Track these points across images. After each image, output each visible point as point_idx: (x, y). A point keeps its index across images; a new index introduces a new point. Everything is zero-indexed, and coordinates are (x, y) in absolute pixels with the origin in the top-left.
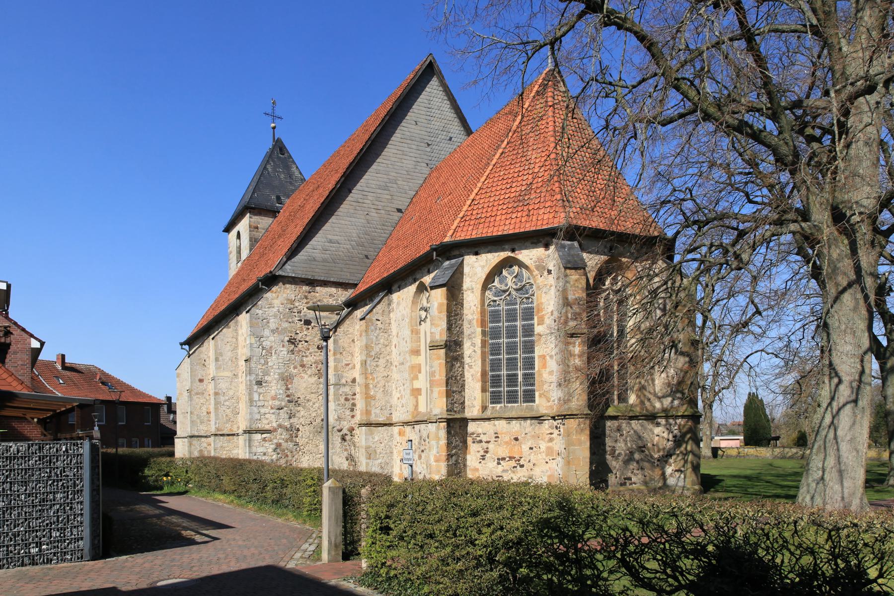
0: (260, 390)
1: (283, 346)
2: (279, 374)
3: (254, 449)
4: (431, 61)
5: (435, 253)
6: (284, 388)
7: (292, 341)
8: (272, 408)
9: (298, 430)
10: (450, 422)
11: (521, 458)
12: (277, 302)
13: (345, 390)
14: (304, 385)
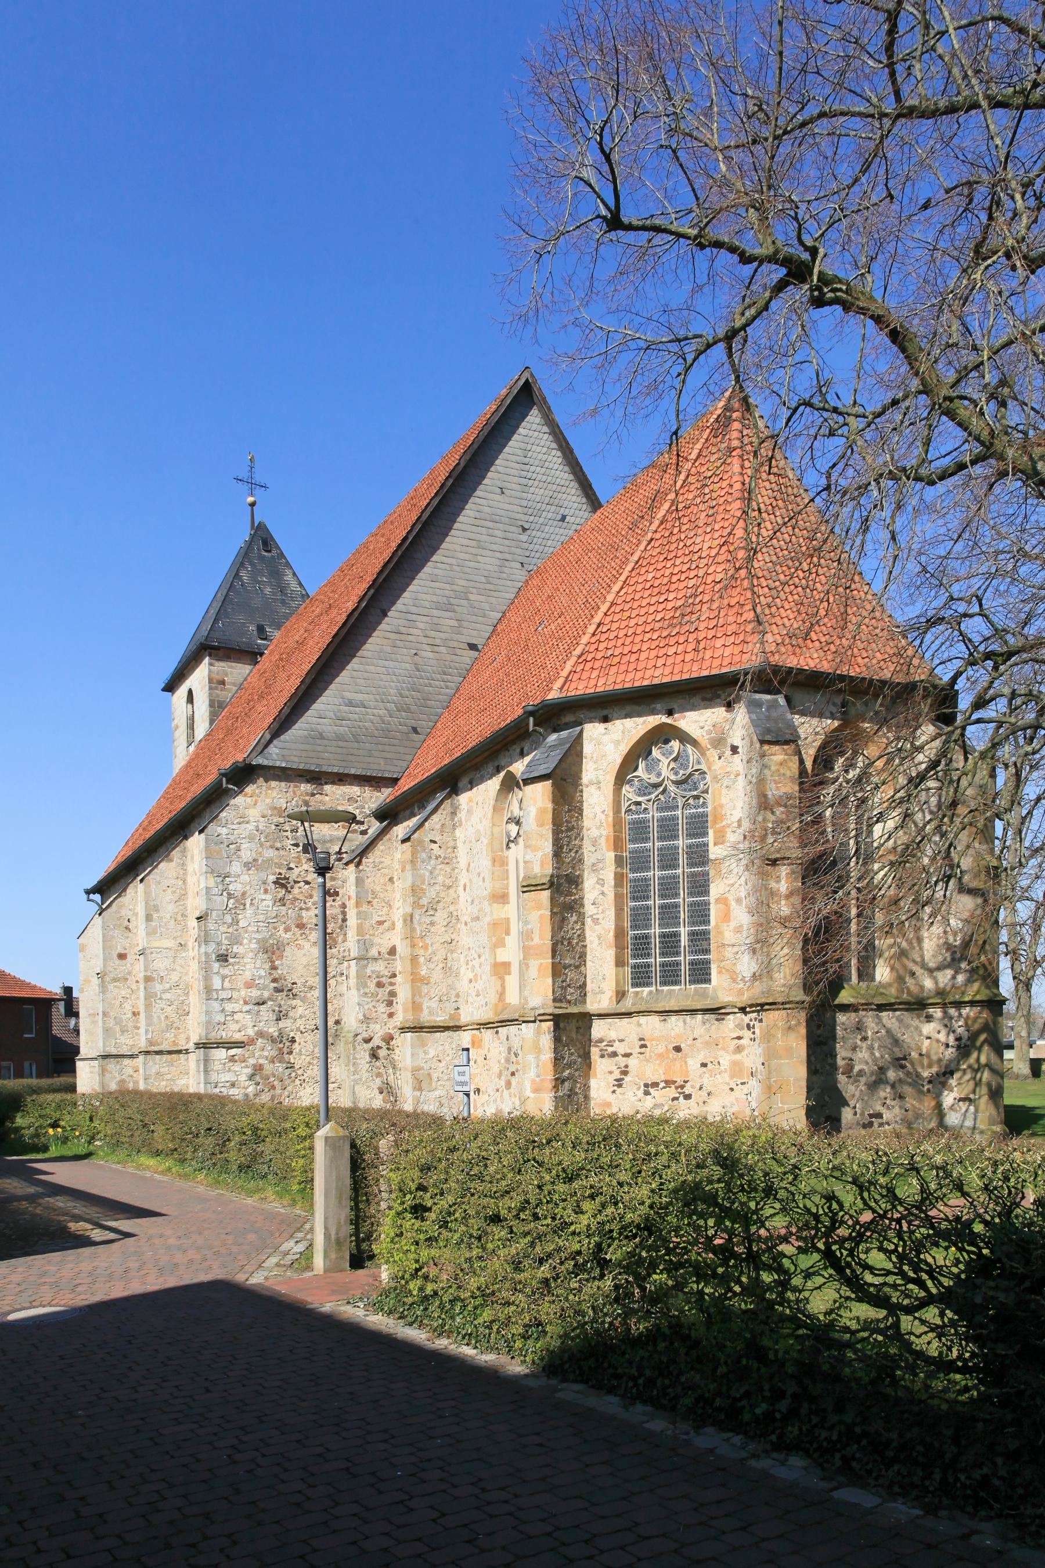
0: (225, 971)
1: (266, 891)
2: (258, 941)
3: (214, 1077)
4: (527, 380)
6: (267, 966)
7: (281, 883)
9: (293, 1041)
10: (558, 1020)
11: (686, 1082)
12: (254, 814)
13: (377, 969)
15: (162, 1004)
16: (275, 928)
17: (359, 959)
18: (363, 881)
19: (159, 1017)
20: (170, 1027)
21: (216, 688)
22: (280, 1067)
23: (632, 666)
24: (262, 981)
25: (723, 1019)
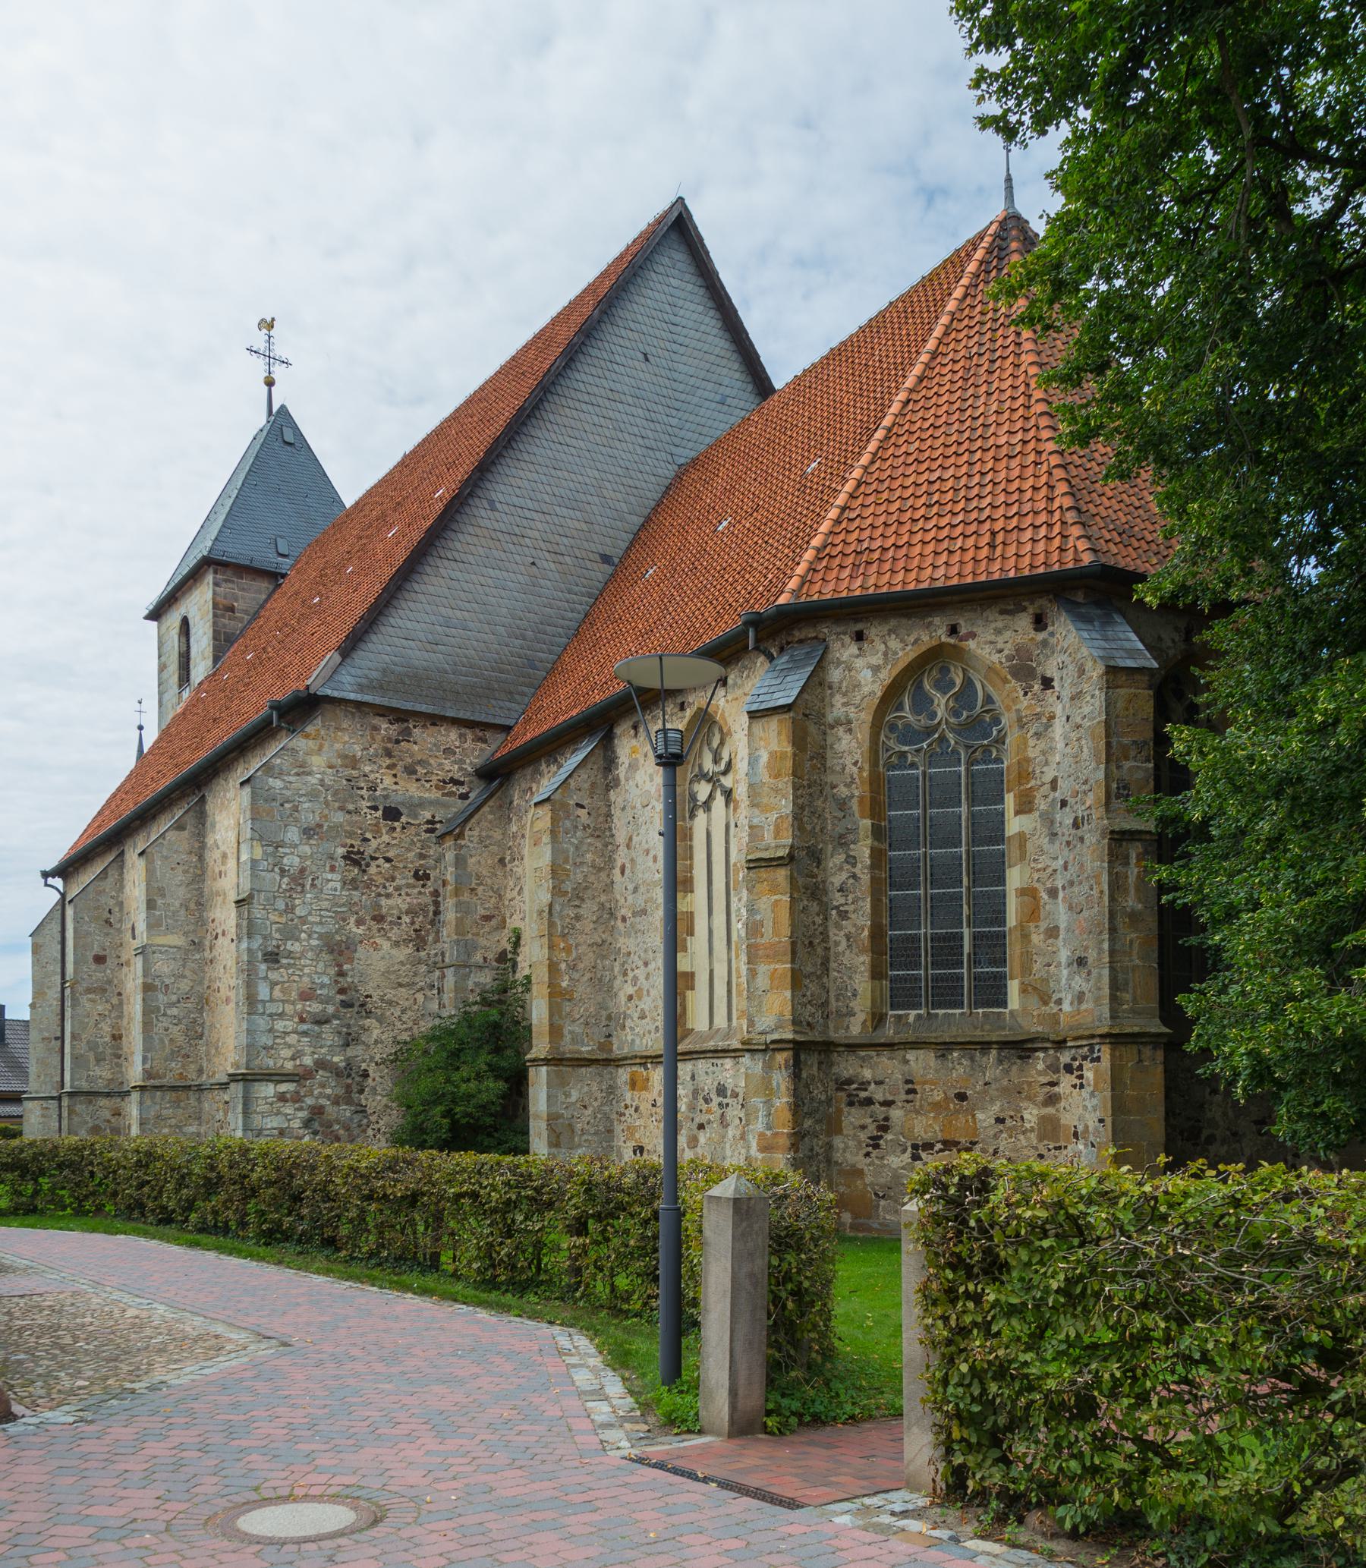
0: (274, 976)
1: (333, 869)
2: (321, 937)
3: (257, 1121)
4: (680, 214)
5: (751, 634)
6: (333, 971)
7: (354, 858)
8: (302, 1020)
9: (365, 1075)
10: (798, 1048)
11: (974, 1143)
12: (317, 762)
13: (482, 980)
14: (382, 966)
15: (165, 1022)
16: (344, 920)
17: (457, 966)
18: (466, 862)
19: (161, 1040)
20: (174, 1055)
21: (223, 616)
22: (346, 1111)
23: (901, 564)
24: (324, 992)
25: (1029, 1057)
